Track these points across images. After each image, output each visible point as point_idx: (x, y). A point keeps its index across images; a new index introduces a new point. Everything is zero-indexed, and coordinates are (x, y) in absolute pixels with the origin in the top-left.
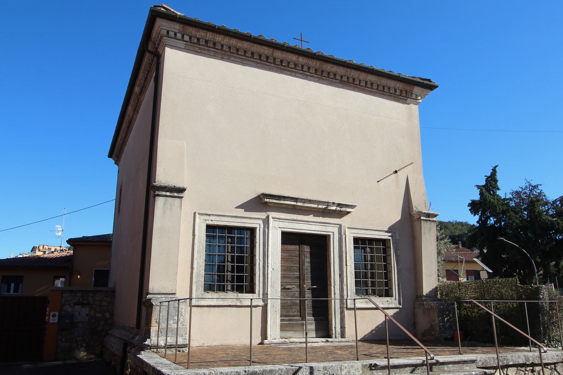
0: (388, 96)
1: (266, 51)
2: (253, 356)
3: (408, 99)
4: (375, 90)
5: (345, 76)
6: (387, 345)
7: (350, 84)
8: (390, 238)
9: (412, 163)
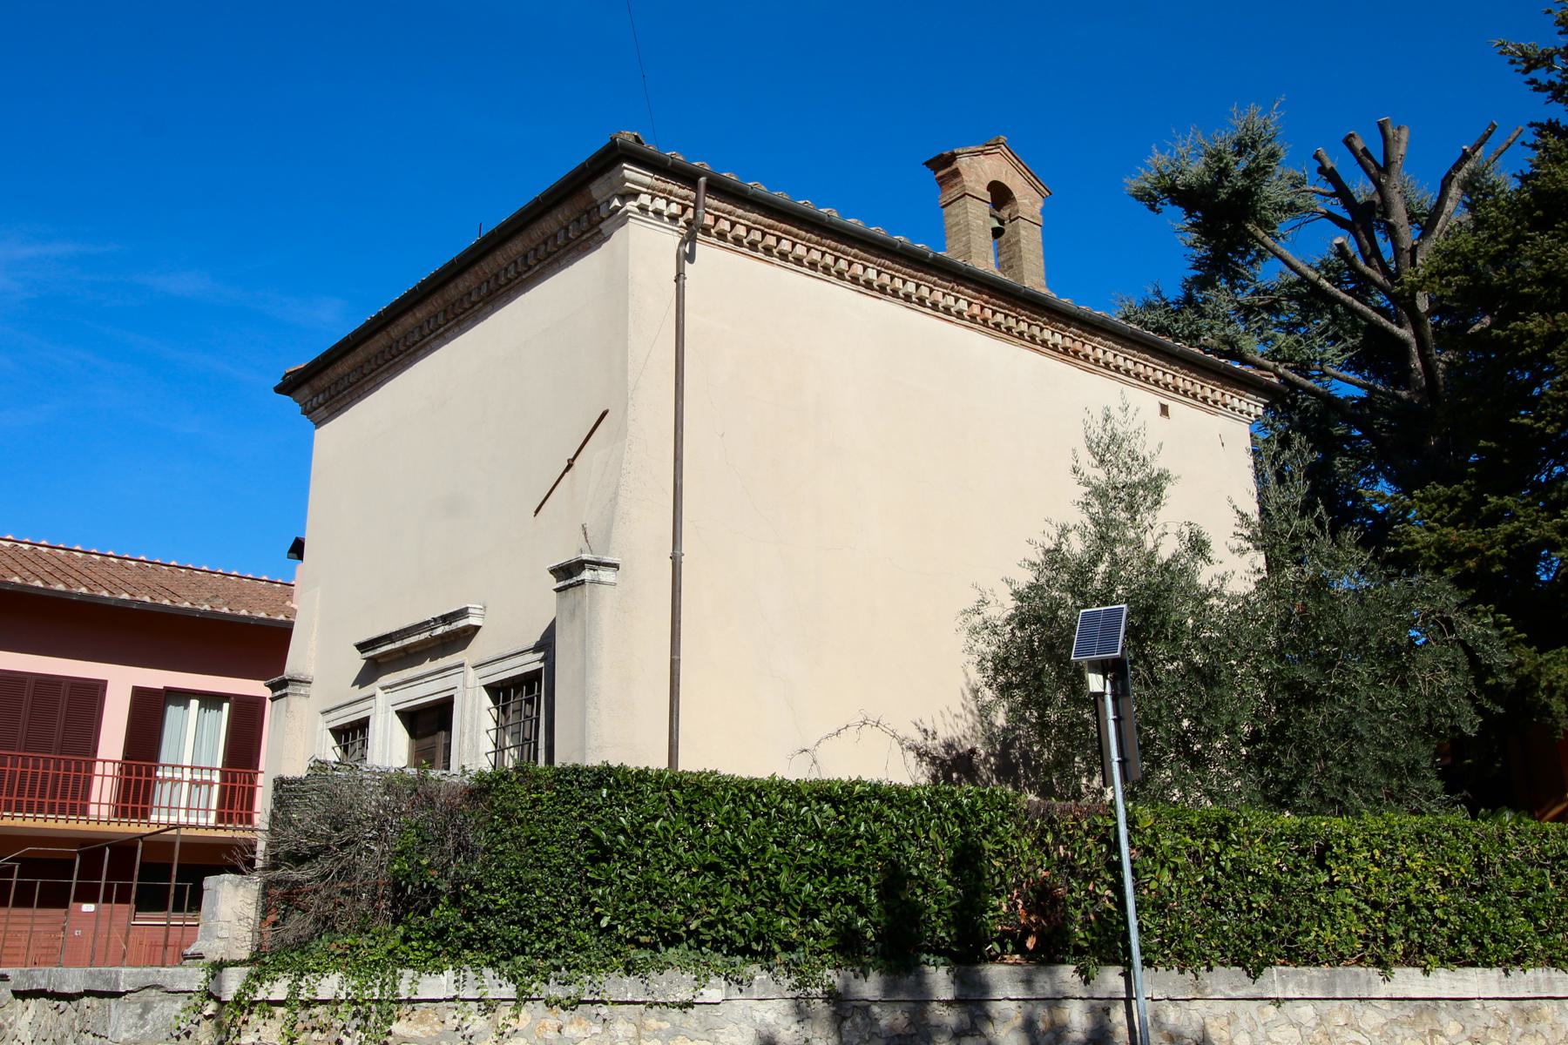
1: (379, 341)
2: (6, 955)
3: (601, 226)
4: (538, 267)
5: (483, 283)
6: (1129, 965)
7: (499, 292)
8: (542, 665)
9: (604, 414)
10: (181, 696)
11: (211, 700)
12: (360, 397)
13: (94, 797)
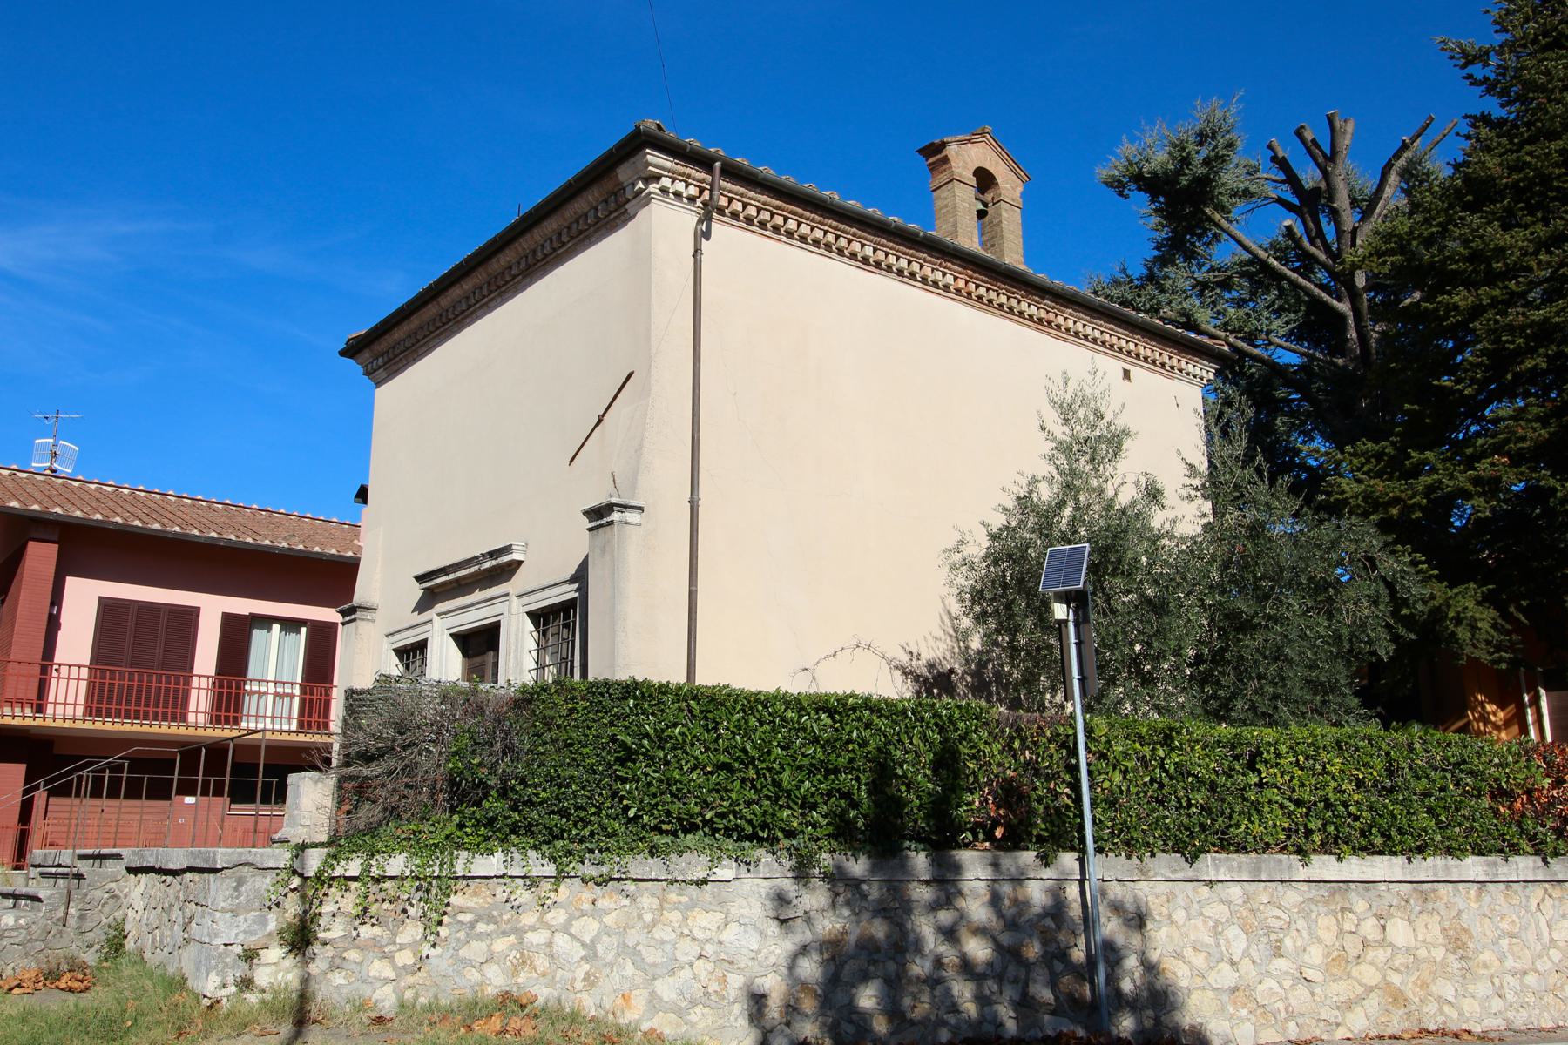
0: (595, 232)
3: (627, 206)
4: (571, 244)
8: (577, 594)
9: (630, 375)
10: (265, 621)
11: (291, 625)
12: (415, 360)
13: (192, 707)
